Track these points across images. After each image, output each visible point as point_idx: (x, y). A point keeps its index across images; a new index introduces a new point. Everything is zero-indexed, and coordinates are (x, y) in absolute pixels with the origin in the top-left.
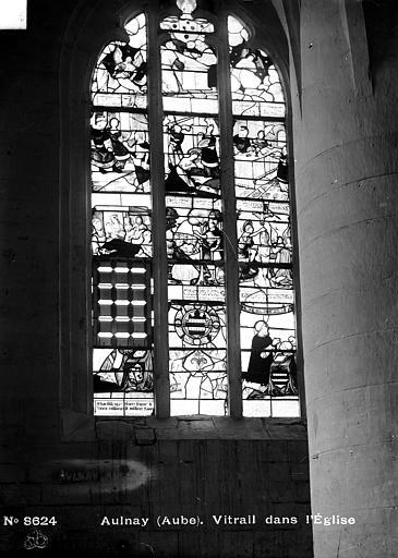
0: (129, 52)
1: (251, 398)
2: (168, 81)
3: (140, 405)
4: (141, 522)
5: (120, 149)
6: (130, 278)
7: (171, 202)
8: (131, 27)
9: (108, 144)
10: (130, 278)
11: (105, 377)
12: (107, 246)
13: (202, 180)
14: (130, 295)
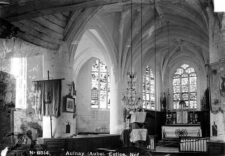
0: (96, 65)
1: (140, 132)
2: (101, 68)
3: (96, 107)
4: (81, 154)
5: (95, 77)
6: (96, 92)
7: (100, 83)
8: (96, 61)
9: (94, 76)
10: (96, 92)
11: (93, 103)
12: (93, 88)
13: (104, 80)
14: (96, 94)
